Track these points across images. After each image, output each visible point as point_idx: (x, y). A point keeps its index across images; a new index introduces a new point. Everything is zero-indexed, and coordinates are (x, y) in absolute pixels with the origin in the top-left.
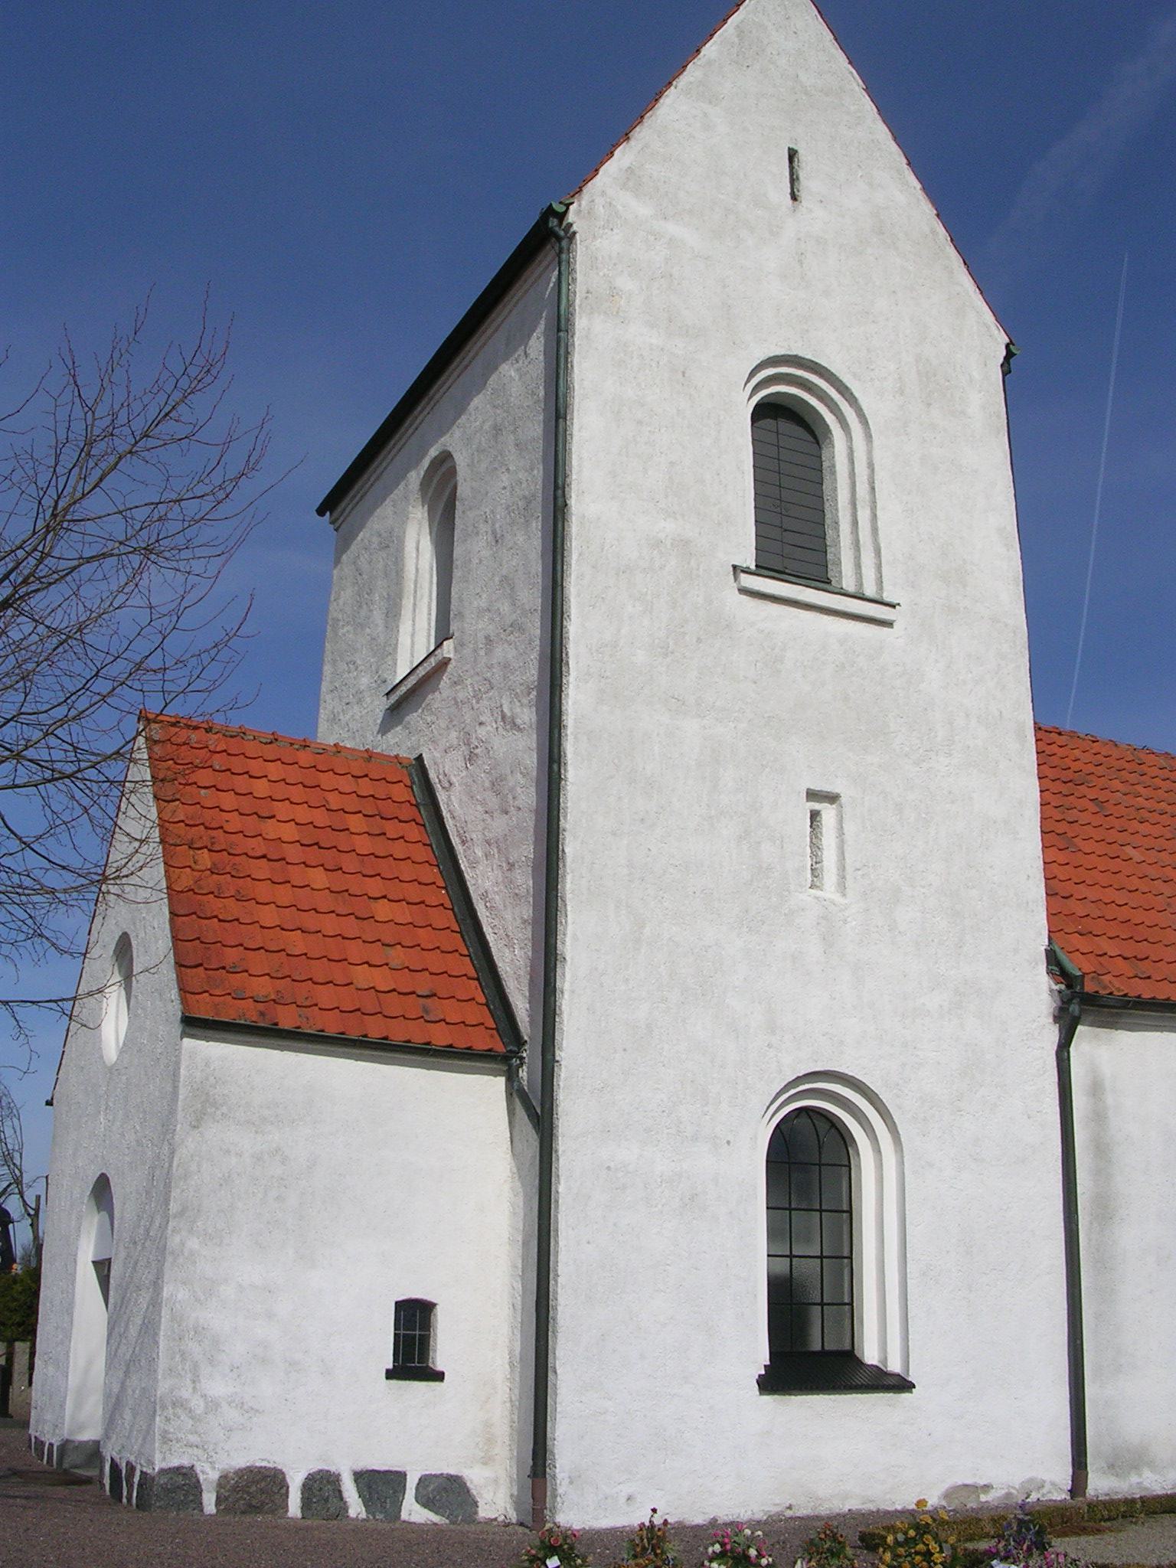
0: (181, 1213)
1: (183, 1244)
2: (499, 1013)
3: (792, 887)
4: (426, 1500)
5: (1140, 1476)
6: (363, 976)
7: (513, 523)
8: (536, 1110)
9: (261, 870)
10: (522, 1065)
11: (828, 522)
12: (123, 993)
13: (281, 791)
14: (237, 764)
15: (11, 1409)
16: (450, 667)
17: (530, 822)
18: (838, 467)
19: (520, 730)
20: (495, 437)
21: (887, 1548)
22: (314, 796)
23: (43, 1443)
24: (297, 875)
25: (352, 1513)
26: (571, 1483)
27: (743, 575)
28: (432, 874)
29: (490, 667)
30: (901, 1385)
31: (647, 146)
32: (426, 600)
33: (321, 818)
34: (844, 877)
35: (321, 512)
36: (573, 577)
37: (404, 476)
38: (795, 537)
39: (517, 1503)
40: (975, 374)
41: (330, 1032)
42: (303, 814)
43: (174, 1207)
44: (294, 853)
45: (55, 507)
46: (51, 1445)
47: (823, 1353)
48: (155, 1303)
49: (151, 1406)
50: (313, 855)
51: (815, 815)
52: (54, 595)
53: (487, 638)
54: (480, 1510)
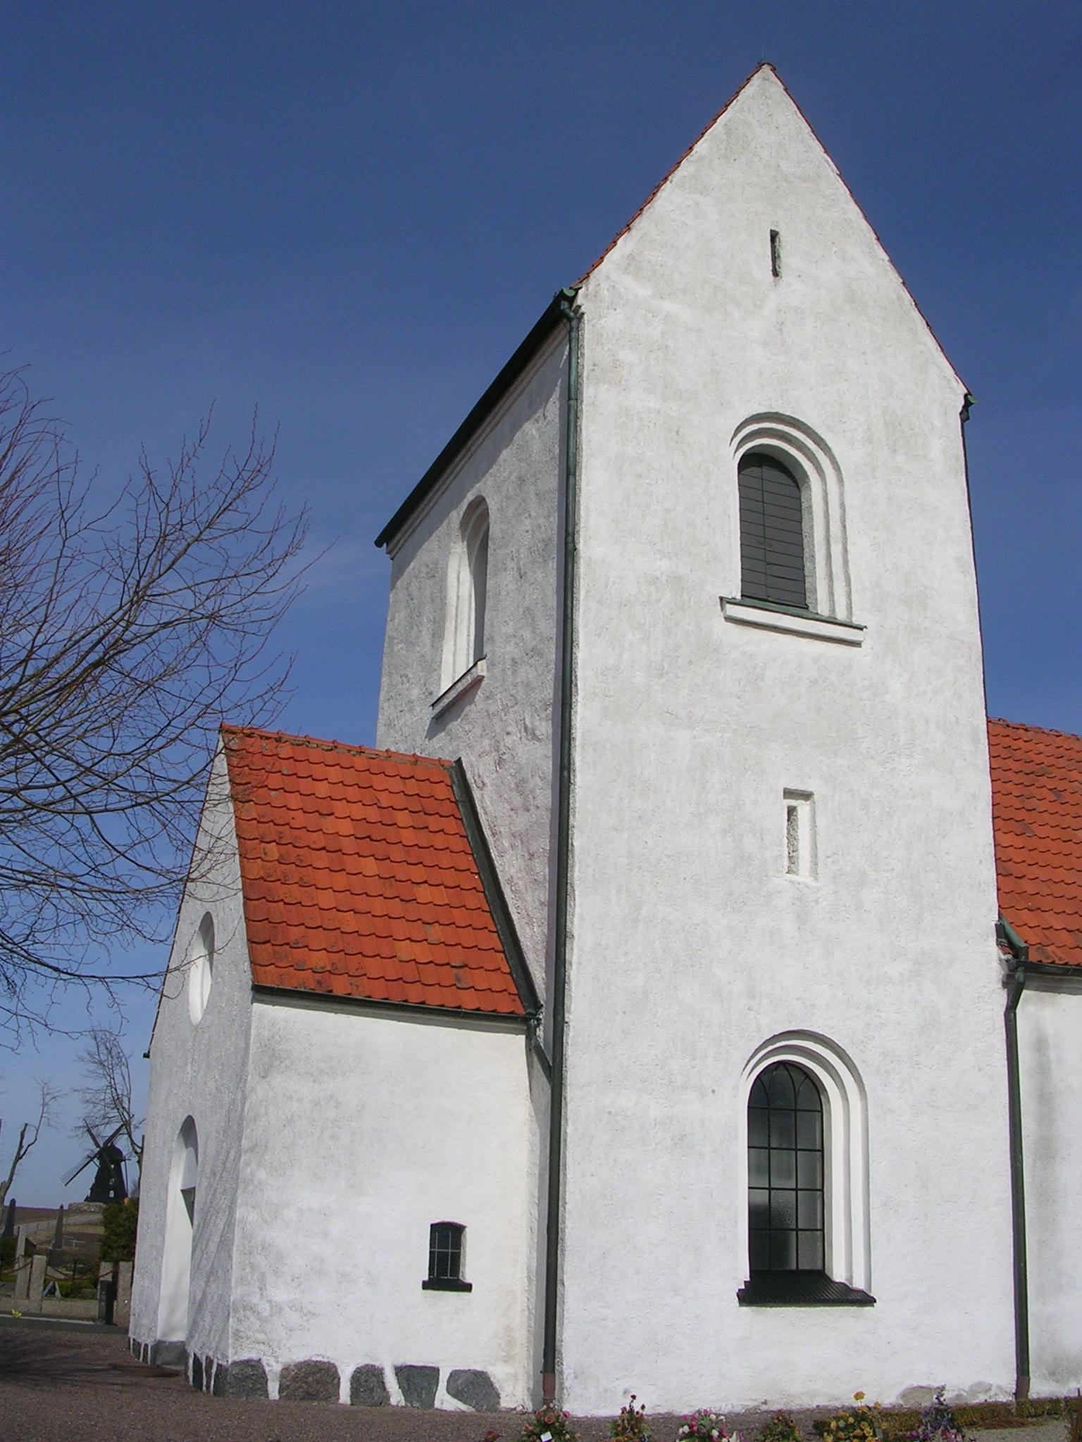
0: (252, 1149)
1: (252, 1174)
2: (522, 982)
3: (771, 873)
4: (455, 1392)
5: (1079, 1382)
6: (405, 950)
7: (534, 562)
8: (550, 1065)
9: (321, 860)
10: (538, 1025)
11: (806, 555)
12: (208, 964)
13: (338, 792)
14: (302, 769)
15: (115, 1320)
16: (484, 684)
17: (547, 820)
18: (815, 508)
19: (539, 740)
20: (520, 486)
21: (829, 1432)
22: (367, 796)
23: (139, 1344)
24: (351, 864)
25: (393, 1401)
26: (576, 1377)
27: (728, 606)
28: (467, 862)
29: (515, 685)
30: (864, 1299)
31: (646, 234)
32: (466, 623)
33: (373, 814)
34: (816, 864)
35: (379, 543)
36: (581, 611)
37: (447, 515)
38: (776, 570)
39: (533, 1396)
40: (937, 423)
41: (377, 997)
42: (357, 811)
43: (245, 1143)
44: (349, 845)
45: (138, 586)
46: (146, 1345)
47: (798, 1272)
48: (230, 1224)
49: (226, 1310)
50: (366, 846)
51: (791, 811)
52: (137, 653)
53: (513, 660)
54: (502, 1401)
